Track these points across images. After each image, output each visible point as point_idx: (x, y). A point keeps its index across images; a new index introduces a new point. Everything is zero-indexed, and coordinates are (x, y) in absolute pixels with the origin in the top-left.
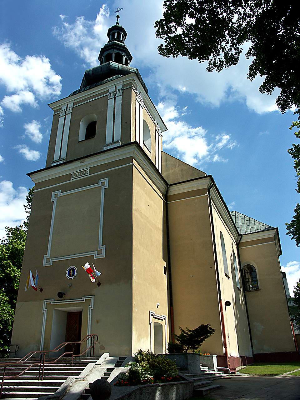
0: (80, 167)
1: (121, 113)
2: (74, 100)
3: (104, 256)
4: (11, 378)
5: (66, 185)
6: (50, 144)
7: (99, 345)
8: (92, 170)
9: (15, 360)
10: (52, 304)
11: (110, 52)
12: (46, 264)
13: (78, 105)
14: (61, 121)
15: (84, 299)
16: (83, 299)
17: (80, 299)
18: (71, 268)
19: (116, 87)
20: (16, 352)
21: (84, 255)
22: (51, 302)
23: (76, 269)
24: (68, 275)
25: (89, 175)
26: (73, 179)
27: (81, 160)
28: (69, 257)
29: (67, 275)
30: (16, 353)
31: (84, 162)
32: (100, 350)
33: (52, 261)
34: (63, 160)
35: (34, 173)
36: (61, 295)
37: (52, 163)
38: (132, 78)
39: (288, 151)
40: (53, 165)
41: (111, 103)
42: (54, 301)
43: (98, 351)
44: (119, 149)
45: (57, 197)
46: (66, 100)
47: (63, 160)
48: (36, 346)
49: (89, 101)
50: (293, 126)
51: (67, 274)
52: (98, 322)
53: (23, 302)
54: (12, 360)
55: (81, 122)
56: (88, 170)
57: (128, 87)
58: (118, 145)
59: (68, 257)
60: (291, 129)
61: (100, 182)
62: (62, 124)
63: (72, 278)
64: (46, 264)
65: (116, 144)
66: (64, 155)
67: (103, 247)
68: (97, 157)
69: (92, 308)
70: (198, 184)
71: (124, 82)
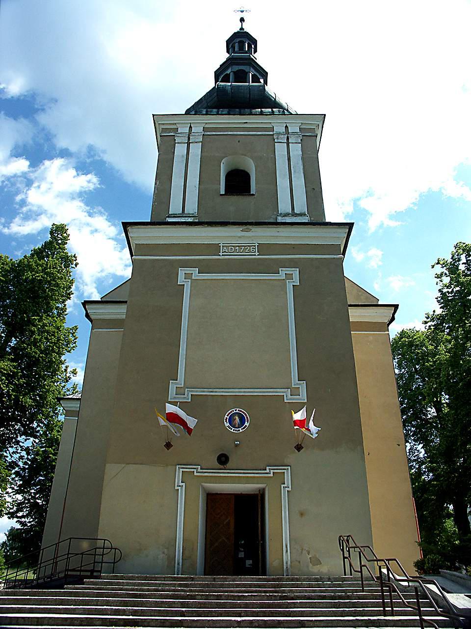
0: (240, 237)
1: (302, 171)
2: (206, 123)
3: (188, 399)
4: (19, 610)
5: (209, 260)
6: (158, 183)
7: (310, 556)
8: (263, 248)
9: (172, 579)
10: (198, 474)
11: (244, 69)
12: (175, 398)
13: (214, 133)
14: (180, 150)
15: (270, 472)
16: (268, 471)
17: (261, 470)
18: (235, 412)
19: (191, 127)
20: (114, 563)
21: (260, 392)
22: (195, 470)
23: (246, 416)
24: (228, 424)
25: (258, 255)
26: (223, 255)
27: (244, 227)
28: (231, 392)
29: (246, 424)
30: (115, 564)
31: (249, 230)
32: (311, 565)
33: (190, 393)
34: (193, 217)
35: (295, 225)
36: (223, 460)
37: (168, 217)
38: (318, 123)
39: (437, 298)
40: (170, 220)
41: (280, 149)
42: (201, 469)
43: (308, 567)
44: (319, 226)
45: (192, 279)
46: (176, 119)
47: (193, 217)
48: (164, 553)
49: (235, 133)
50: (437, 264)
51: (226, 421)
52: (302, 514)
53: (123, 465)
54: (165, 578)
55: (222, 163)
56: (255, 246)
57: (310, 134)
58: (305, 219)
59: (252, 390)
60: (433, 267)
61: (283, 273)
62: (183, 156)
63: (239, 430)
64: (175, 398)
65: (300, 217)
66: (192, 207)
67: (300, 384)
68: (277, 229)
69: (290, 489)
70: (375, 314)
71: (302, 123)
